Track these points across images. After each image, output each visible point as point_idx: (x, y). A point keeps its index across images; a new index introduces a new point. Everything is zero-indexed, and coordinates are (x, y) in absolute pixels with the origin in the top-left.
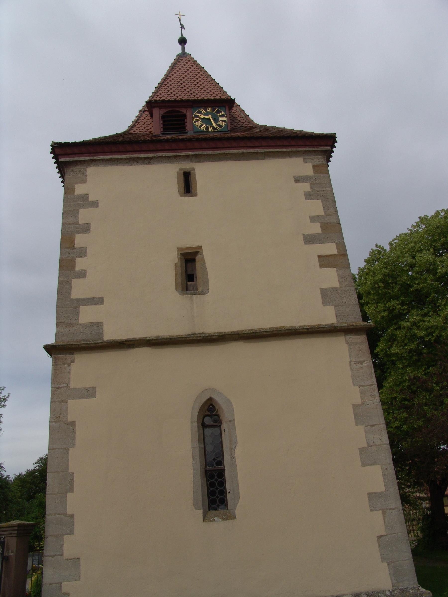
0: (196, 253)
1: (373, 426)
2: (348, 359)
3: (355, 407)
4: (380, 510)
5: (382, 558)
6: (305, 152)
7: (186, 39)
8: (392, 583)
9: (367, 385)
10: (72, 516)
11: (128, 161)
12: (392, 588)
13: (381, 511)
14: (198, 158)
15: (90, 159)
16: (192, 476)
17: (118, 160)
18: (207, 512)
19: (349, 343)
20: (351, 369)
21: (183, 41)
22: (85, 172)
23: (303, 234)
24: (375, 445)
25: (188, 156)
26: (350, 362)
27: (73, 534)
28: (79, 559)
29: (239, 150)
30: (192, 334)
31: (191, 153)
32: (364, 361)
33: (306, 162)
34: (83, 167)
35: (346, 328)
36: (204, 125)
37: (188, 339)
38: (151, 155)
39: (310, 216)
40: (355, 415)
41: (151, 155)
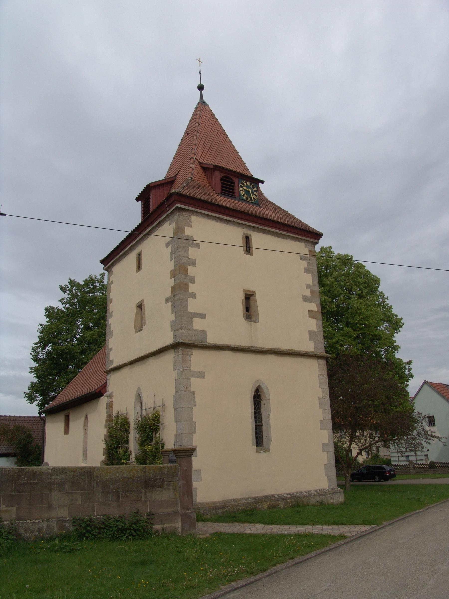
0: (252, 295)
1: (326, 409)
2: (318, 373)
3: (320, 399)
5: (325, 474)
6: (307, 240)
11: (216, 219)
13: (326, 452)
14: (255, 229)
15: (195, 210)
17: (211, 216)
20: (319, 378)
21: (201, 88)
22: (190, 219)
23: (302, 295)
25: (249, 226)
26: (319, 374)
27: (197, 456)
28: (200, 470)
29: (276, 230)
33: (306, 247)
34: (189, 214)
35: (320, 356)
36: (245, 195)
37: (252, 350)
39: (306, 284)
40: (320, 403)
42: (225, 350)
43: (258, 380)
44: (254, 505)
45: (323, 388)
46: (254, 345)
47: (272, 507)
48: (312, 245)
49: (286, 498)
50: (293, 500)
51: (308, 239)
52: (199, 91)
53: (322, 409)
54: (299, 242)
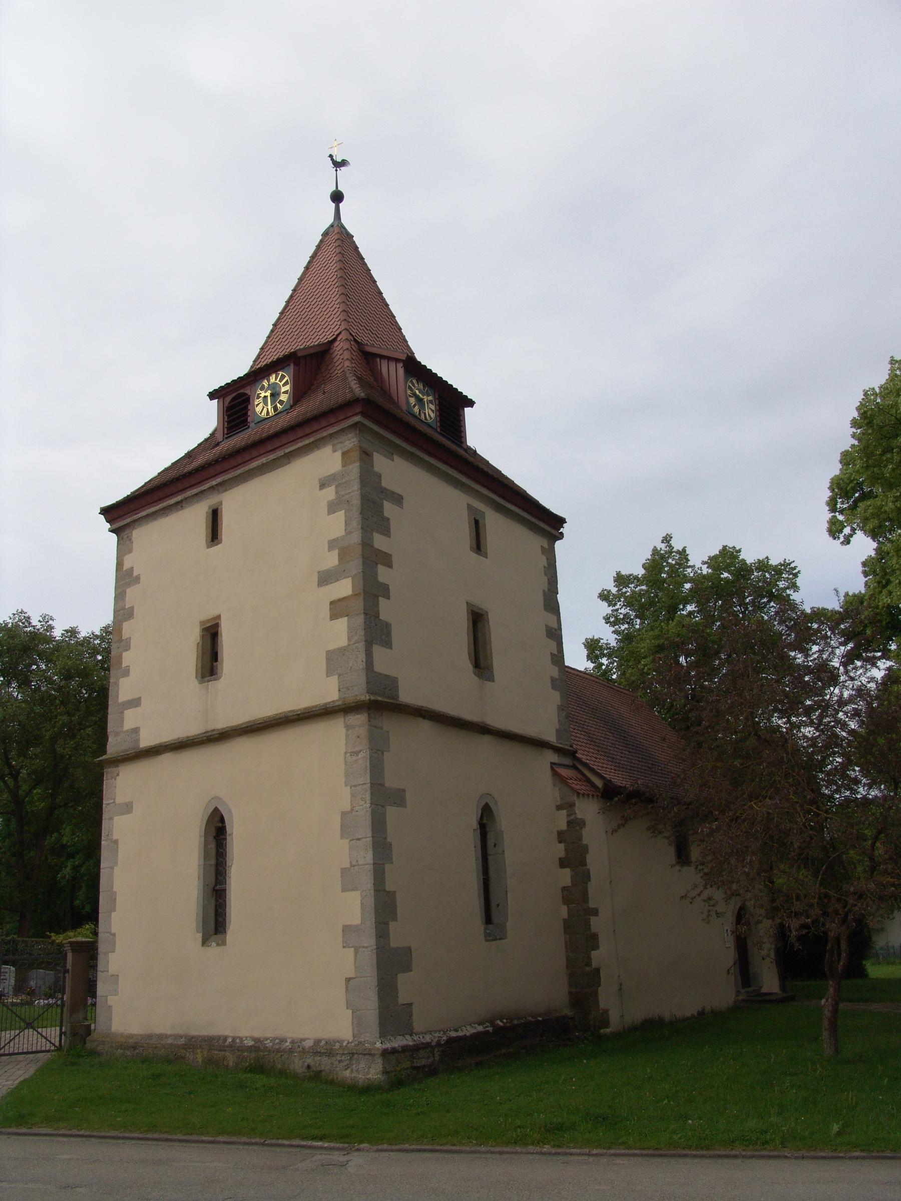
1: (359, 839)
2: (344, 750)
3: (344, 814)
4: (352, 947)
7: (342, 194)
8: (353, 1034)
9: (360, 785)
10: (114, 935)
12: (352, 1038)
13: (353, 949)
14: (224, 486)
16: (196, 896)
17: (154, 513)
18: (211, 936)
19: (348, 727)
20: (346, 762)
21: (337, 197)
24: (359, 865)
25: (212, 488)
26: (346, 753)
30: (205, 733)
31: (214, 483)
32: (360, 751)
38: (179, 498)
40: (343, 825)
41: (179, 498)
42: (163, 753)
43: (213, 798)
44: (182, 1051)
45: (355, 786)
46: (210, 728)
47: (209, 1061)
48: (350, 435)
49: (242, 1049)
50: (253, 1055)
51: (331, 430)
52: (334, 204)
53: (348, 840)
54: (319, 449)
